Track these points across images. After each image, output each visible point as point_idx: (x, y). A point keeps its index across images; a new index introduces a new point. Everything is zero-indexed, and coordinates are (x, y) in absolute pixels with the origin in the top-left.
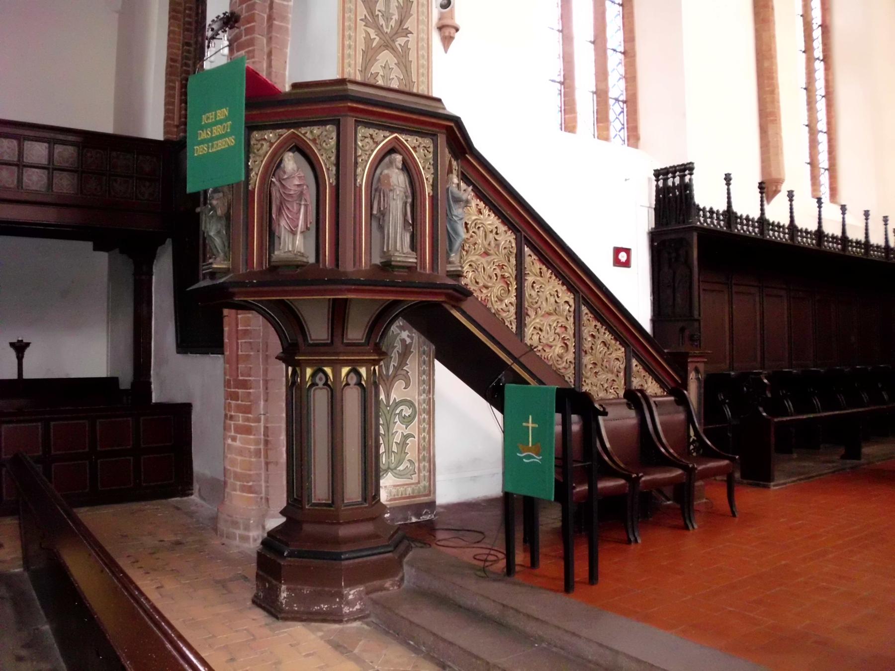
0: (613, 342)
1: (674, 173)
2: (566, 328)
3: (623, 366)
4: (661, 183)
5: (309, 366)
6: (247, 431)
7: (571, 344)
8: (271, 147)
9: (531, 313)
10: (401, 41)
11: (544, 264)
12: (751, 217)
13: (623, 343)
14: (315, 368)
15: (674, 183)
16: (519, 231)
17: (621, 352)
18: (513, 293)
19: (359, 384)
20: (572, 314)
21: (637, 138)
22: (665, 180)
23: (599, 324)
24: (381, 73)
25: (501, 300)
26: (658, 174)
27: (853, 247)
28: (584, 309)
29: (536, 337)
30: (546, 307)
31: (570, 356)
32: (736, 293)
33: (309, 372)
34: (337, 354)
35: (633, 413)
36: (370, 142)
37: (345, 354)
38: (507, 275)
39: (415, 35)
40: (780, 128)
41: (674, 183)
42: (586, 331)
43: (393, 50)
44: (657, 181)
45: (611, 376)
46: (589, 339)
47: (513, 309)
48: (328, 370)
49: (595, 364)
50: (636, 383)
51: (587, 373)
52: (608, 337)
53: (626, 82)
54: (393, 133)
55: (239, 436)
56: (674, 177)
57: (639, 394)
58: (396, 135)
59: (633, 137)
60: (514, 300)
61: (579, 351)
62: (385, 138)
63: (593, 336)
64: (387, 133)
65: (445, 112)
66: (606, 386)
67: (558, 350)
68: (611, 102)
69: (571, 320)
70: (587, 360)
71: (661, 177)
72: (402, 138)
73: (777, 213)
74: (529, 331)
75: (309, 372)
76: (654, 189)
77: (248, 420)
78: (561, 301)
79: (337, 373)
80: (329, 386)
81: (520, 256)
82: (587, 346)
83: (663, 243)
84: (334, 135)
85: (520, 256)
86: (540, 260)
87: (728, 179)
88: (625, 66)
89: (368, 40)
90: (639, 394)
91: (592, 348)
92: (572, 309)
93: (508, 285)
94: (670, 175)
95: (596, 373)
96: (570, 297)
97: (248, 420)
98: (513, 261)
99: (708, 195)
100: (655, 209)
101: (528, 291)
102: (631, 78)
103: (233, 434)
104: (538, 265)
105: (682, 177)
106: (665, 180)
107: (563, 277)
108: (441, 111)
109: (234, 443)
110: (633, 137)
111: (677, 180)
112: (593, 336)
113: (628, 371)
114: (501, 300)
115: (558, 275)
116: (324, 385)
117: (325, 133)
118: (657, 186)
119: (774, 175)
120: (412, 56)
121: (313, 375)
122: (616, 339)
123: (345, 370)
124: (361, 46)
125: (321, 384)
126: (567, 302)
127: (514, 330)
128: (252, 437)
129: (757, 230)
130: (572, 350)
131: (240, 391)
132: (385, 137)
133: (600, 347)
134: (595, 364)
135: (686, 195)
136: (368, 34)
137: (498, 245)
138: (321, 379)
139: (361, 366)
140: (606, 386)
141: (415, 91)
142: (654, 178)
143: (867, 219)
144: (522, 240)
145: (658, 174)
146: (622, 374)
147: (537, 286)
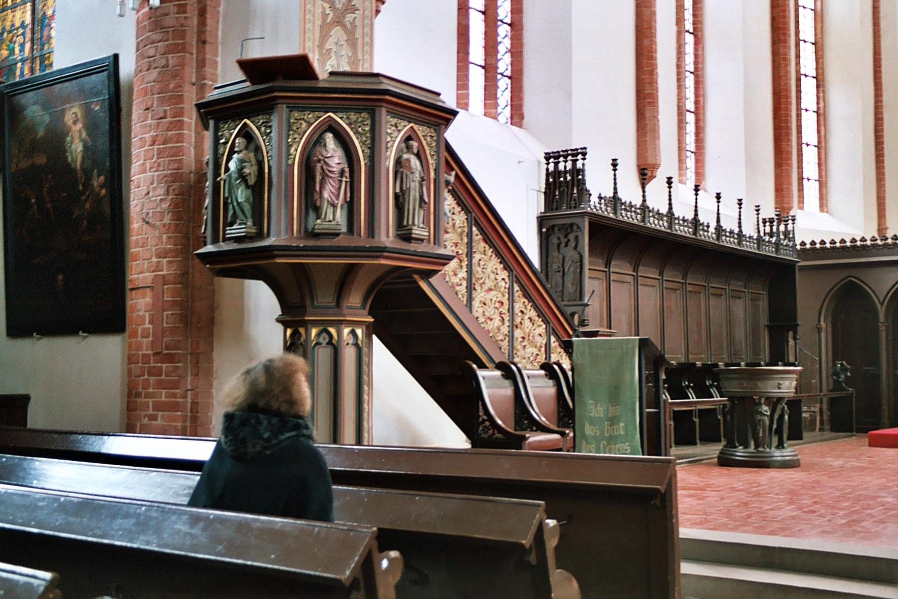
0: (537, 318)
1: (566, 157)
2: (502, 303)
3: (544, 342)
4: (551, 167)
5: (315, 327)
6: (175, 407)
7: (507, 318)
8: (309, 127)
9: (478, 287)
10: (349, 17)
11: (487, 243)
12: (633, 204)
13: (545, 321)
14: (321, 328)
15: (565, 167)
16: (470, 213)
17: (542, 329)
18: (465, 269)
19: (356, 345)
20: (507, 290)
21: (522, 117)
22: (556, 164)
23: (526, 301)
24: (334, 50)
25: (456, 275)
26: (548, 157)
27: (727, 236)
28: (516, 288)
29: (481, 310)
30: (489, 284)
31: (505, 330)
32: (614, 281)
33: (314, 332)
34: (343, 315)
35: (551, 383)
36: (394, 133)
37: (350, 315)
38: (460, 252)
39: (361, 12)
40: (657, 112)
41: (565, 167)
42: (518, 306)
43: (344, 26)
44: (548, 164)
45: (535, 351)
46: (520, 314)
47: (464, 283)
48: (332, 330)
49: (523, 338)
50: (554, 358)
51: (518, 346)
52: (533, 313)
53: (512, 57)
54: (410, 122)
55: (160, 413)
56: (566, 162)
57: (556, 367)
58: (412, 124)
59: (517, 116)
60: (465, 275)
61: (513, 326)
62: (406, 127)
63: (522, 312)
64: (406, 123)
65: (445, 106)
66: (532, 359)
67: (497, 322)
68: (499, 76)
69: (507, 296)
70: (518, 333)
71: (552, 160)
72: (416, 127)
73: (657, 200)
74: (476, 304)
75: (314, 332)
76: (545, 172)
77: (174, 395)
78: (499, 278)
79: (339, 334)
80: (333, 345)
81: (470, 235)
82: (518, 320)
83: (551, 229)
84: (369, 122)
85: (470, 235)
86: (484, 240)
87: (615, 165)
88: (511, 39)
89: (325, 15)
90: (556, 367)
91: (521, 323)
92: (507, 286)
93: (461, 261)
94: (561, 159)
95: (525, 346)
96: (504, 274)
97: (174, 395)
98: (465, 240)
99: (597, 184)
100: (545, 193)
101: (476, 269)
102: (517, 52)
103: (151, 412)
104: (483, 244)
105: (574, 162)
106: (556, 164)
107: (502, 257)
108: (439, 104)
109: (154, 422)
110: (517, 116)
111: (569, 165)
112: (522, 312)
113: (548, 346)
114: (456, 275)
115: (498, 254)
116: (328, 344)
117: (360, 120)
118: (547, 169)
119: (650, 160)
120: (358, 35)
121: (318, 335)
122: (539, 316)
123: (346, 331)
124: (319, 22)
125: (324, 343)
126: (503, 279)
127: (465, 303)
128: (179, 413)
129: (639, 217)
130: (507, 324)
131: (164, 365)
132: (405, 126)
133: (527, 323)
134: (523, 338)
135: (579, 180)
136: (323, 8)
137: (454, 225)
138: (324, 339)
139: (358, 328)
140: (532, 359)
141: (360, 70)
142: (545, 161)
143: (670, 187)
144: (472, 221)
145: (548, 157)
146: (543, 349)
147: (482, 263)
